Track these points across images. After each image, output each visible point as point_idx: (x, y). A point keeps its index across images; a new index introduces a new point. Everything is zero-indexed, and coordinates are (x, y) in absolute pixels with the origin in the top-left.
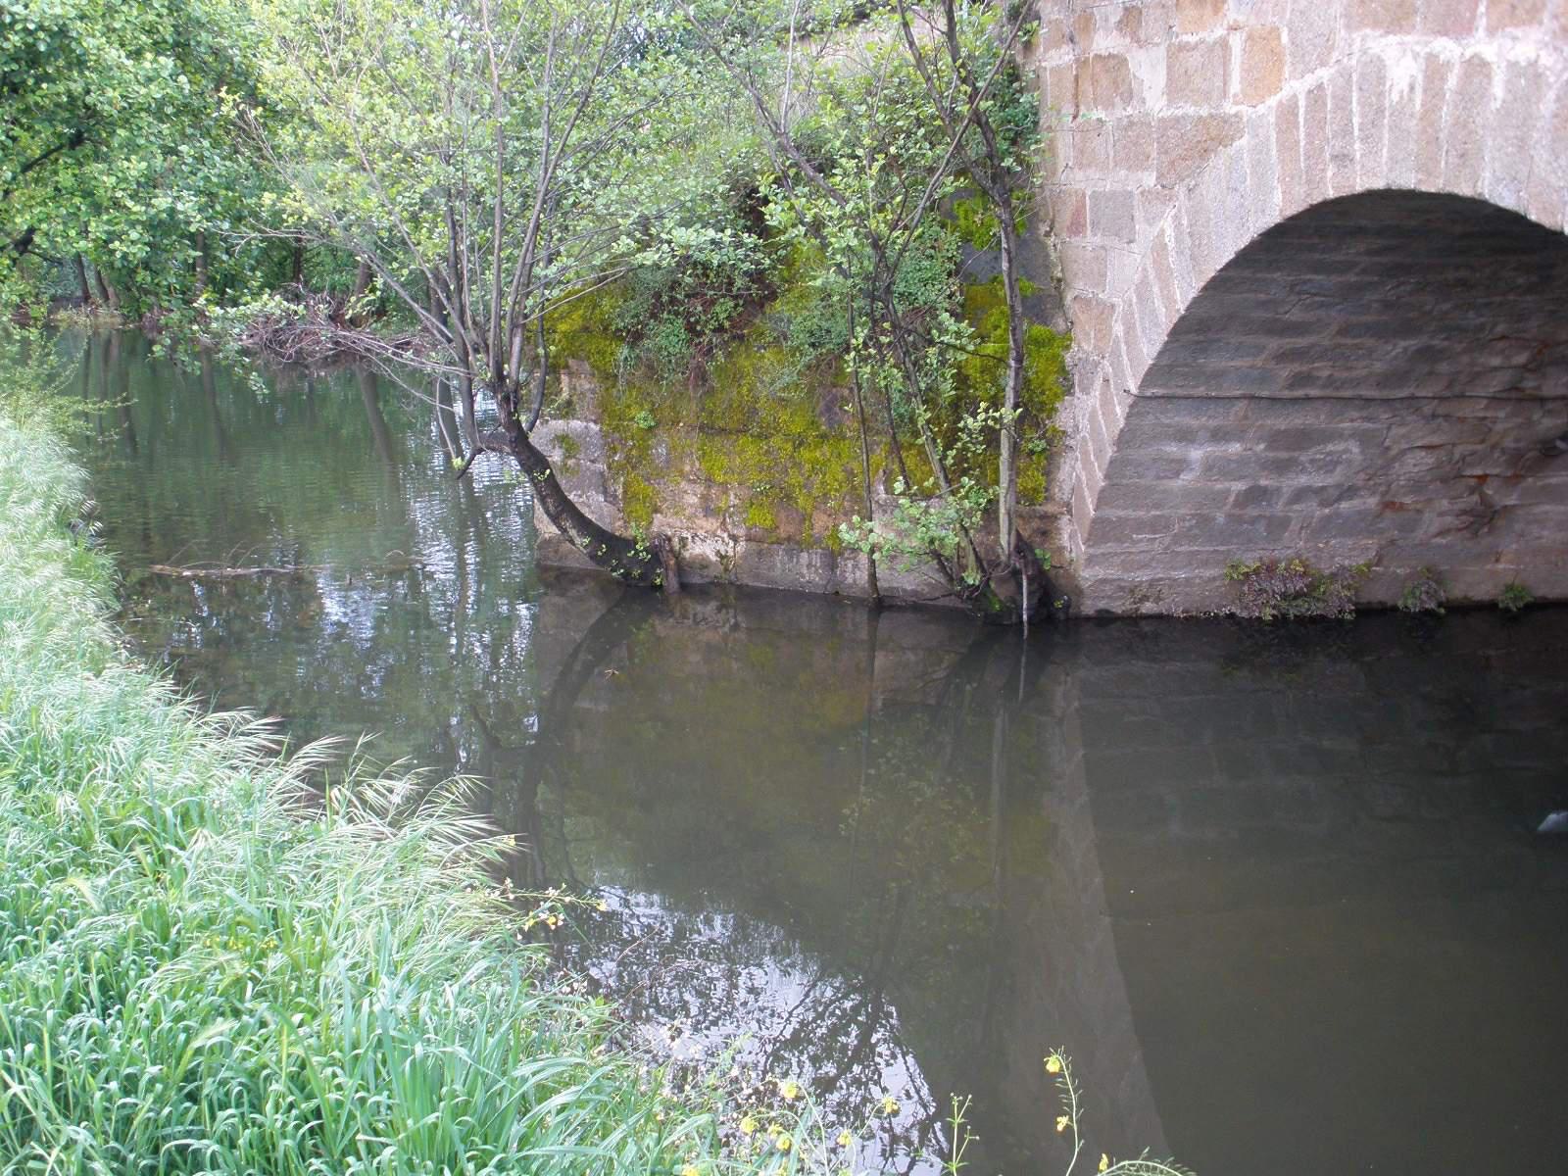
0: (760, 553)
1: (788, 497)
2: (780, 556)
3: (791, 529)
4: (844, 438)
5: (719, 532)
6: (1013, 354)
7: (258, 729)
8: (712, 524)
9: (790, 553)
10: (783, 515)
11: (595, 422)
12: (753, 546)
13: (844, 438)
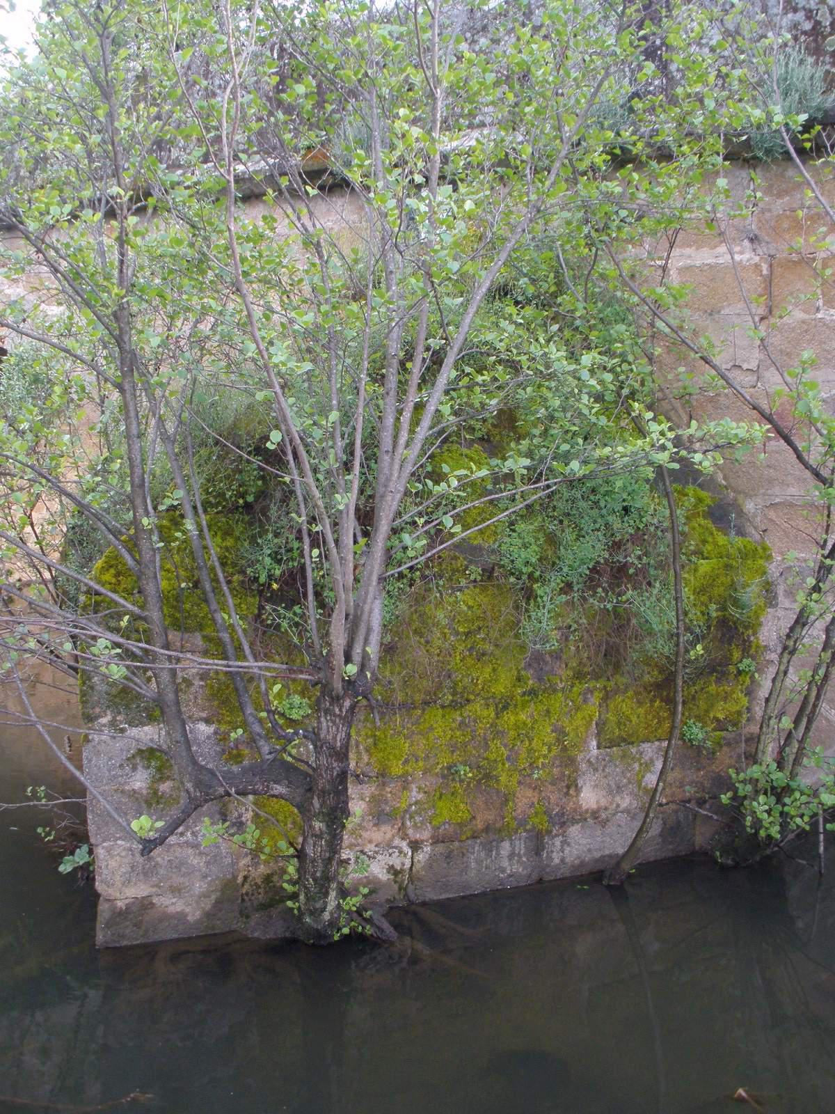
0: (448, 856)
1: (488, 776)
2: (476, 854)
3: (490, 816)
4: (555, 691)
5: (397, 842)
6: (794, 756)
7: (547, 878)
8: (386, 832)
9: (488, 848)
10: (480, 802)
11: (208, 721)
12: (440, 848)
13: (555, 691)
